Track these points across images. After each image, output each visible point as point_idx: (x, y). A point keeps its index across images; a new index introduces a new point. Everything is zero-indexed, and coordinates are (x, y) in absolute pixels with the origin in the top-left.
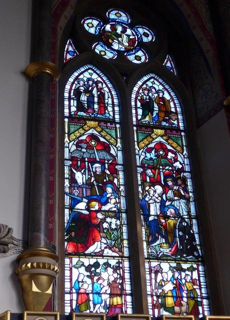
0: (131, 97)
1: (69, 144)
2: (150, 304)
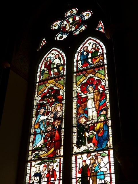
0: (107, 59)
1: (76, 88)
2: (111, 139)
